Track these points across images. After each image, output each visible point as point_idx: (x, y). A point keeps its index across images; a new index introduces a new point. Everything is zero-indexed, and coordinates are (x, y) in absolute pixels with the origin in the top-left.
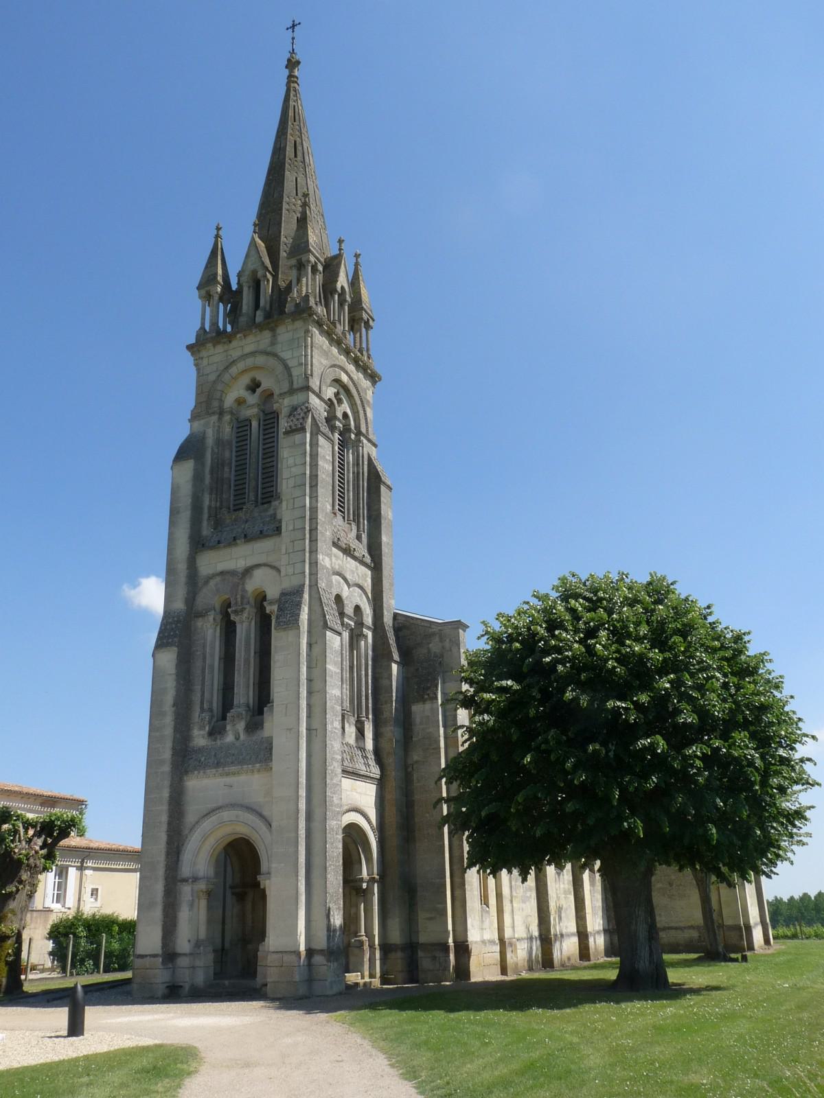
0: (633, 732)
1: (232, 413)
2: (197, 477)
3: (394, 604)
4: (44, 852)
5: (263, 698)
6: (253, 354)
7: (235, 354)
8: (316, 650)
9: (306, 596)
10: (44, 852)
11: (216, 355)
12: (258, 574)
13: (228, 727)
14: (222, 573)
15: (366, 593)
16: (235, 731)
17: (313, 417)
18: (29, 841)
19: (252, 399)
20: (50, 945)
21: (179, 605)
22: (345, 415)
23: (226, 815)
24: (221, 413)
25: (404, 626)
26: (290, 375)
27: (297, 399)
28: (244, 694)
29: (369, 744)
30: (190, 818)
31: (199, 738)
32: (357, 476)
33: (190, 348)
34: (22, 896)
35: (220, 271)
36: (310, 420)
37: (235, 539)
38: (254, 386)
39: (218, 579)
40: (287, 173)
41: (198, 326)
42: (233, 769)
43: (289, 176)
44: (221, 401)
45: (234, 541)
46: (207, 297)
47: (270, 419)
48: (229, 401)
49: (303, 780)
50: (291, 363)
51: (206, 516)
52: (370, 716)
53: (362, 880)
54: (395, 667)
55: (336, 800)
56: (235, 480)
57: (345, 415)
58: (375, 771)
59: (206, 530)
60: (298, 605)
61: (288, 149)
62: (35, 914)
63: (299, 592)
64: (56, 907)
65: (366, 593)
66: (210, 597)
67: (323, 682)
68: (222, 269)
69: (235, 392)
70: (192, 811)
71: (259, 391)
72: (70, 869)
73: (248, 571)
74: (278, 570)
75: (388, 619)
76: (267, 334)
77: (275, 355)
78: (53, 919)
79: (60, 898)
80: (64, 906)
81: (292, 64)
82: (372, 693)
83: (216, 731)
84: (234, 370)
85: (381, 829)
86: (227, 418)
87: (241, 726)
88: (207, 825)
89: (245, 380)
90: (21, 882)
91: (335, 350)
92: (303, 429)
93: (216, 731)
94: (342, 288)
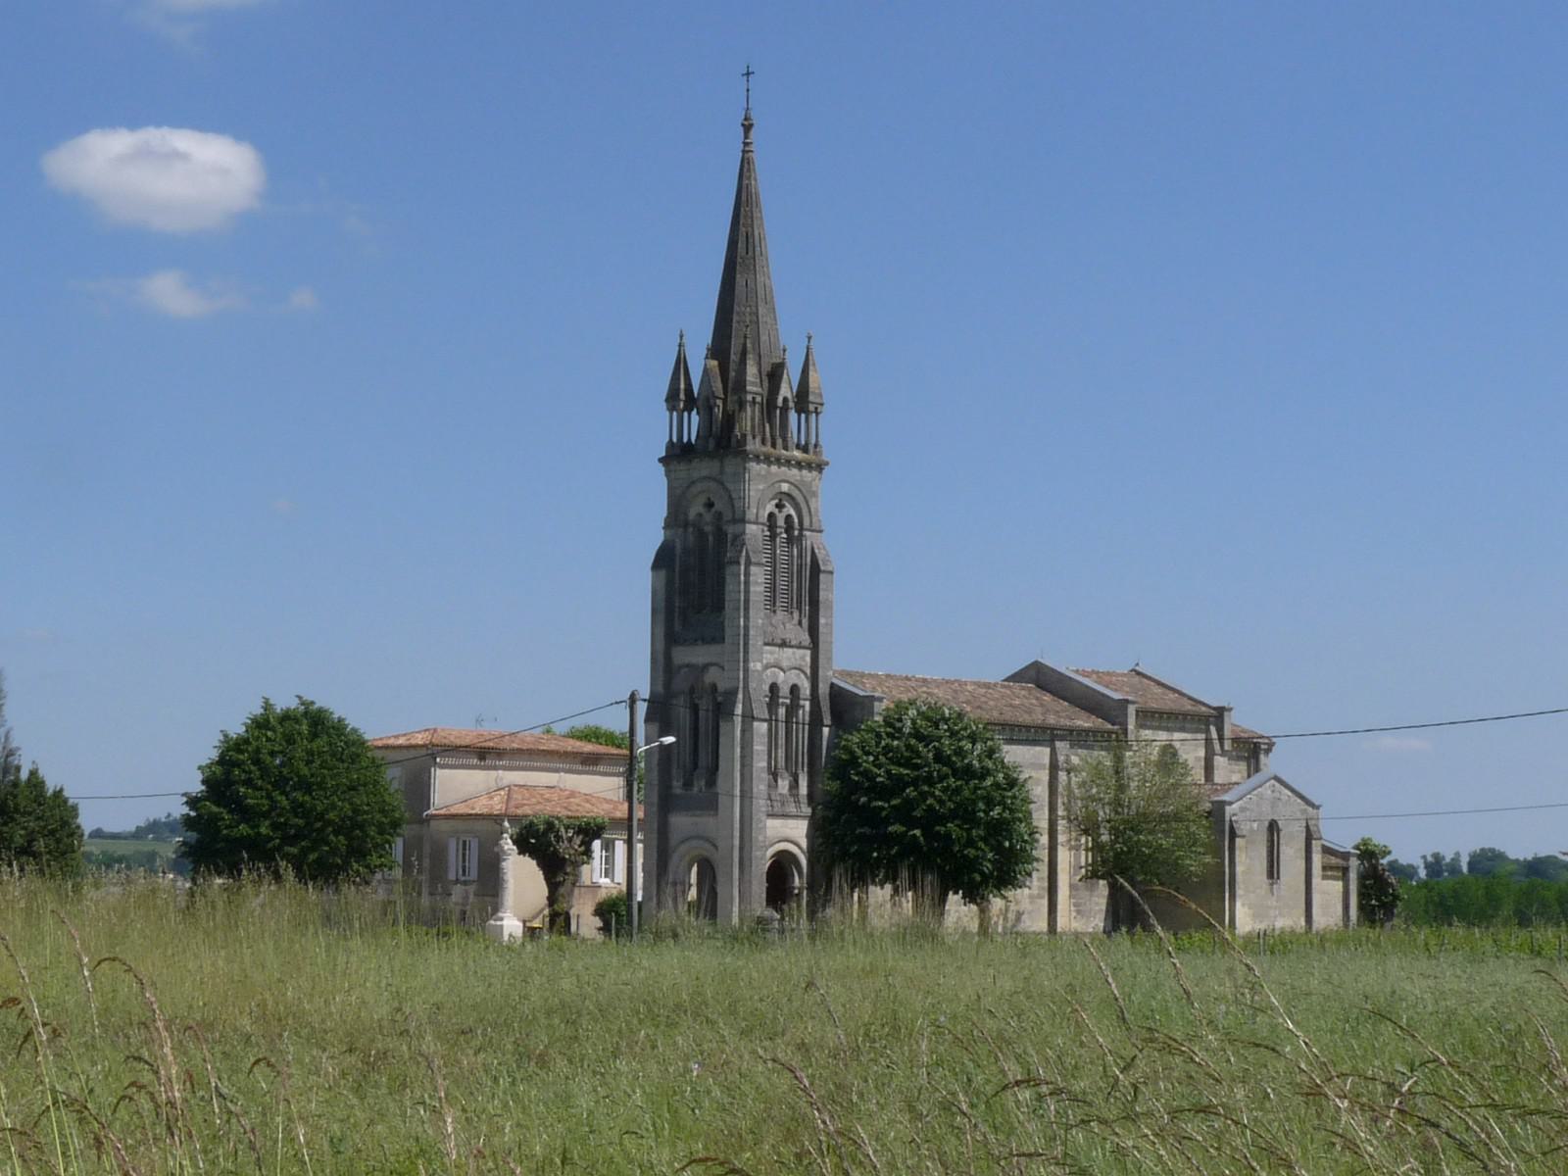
0: (887, 821)
1: (694, 525)
2: (669, 583)
3: (827, 676)
4: (583, 848)
5: (714, 769)
6: (705, 478)
7: (696, 475)
8: (747, 735)
9: (740, 696)
10: (583, 848)
11: (555, 930)
12: (713, 670)
13: (695, 783)
14: (688, 666)
15: (805, 674)
16: (699, 784)
17: (747, 553)
18: (570, 840)
19: (708, 517)
20: (598, 922)
21: (660, 689)
22: (788, 518)
23: (694, 843)
24: (686, 525)
25: (836, 693)
26: (733, 506)
27: (737, 528)
28: (704, 759)
29: (803, 789)
30: (673, 842)
31: (677, 787)
32: (800, 566)
33: (661, 460)
34: (568, 884)
35: (682, 386)
36: (744, 553)
37: (696, 640)
38: (710, 505)
39: (686, 669)
40: (738, 276)
41: (667, 439)
42: (699, 812)
43: (740, 280)
44: (686, 514)
45: (695, 642)
46: (672, 408)
47: (720, 535)
48: (692, 514)
49: (737, 825)
50: (734, 496)
51: (676, 615)
52: (806, 769)
53: (794, 888)
54: (826, 731)
55: (761, 838)
56: (694, 585)
57: (788, 518)
58: (808, 811)
59: (678, 627)
60: (734, 704)
61: (739, 245)
62: (583, 889)
63: (735, 692)
64: (604, 881)
65: (805, 674)
66: (681, 683)
67: (754, 748)
68: (685, 384)
69: (696, 509)
70: (674, 838)
71: (713, 510)
72: (617, 842)
73: (706, 667)
74: (723, 668)
75: (824, 689)
76: (716, 464)
77: (722, 484)
78: (602, 895)
79: (609, 872)
80: (613, 881)
81: (747, 128)
82: (644, 865)
83: (688, 785)
84: (694, 490)
85: (812, 853)
86: (691, 529)
87: (703, 783)
88: (683, 848)
89: (702, 499)
90: (566, 874)
91: (774, 468)
92: (739, 563)
93: (688, 785)
94: (785, 400)
